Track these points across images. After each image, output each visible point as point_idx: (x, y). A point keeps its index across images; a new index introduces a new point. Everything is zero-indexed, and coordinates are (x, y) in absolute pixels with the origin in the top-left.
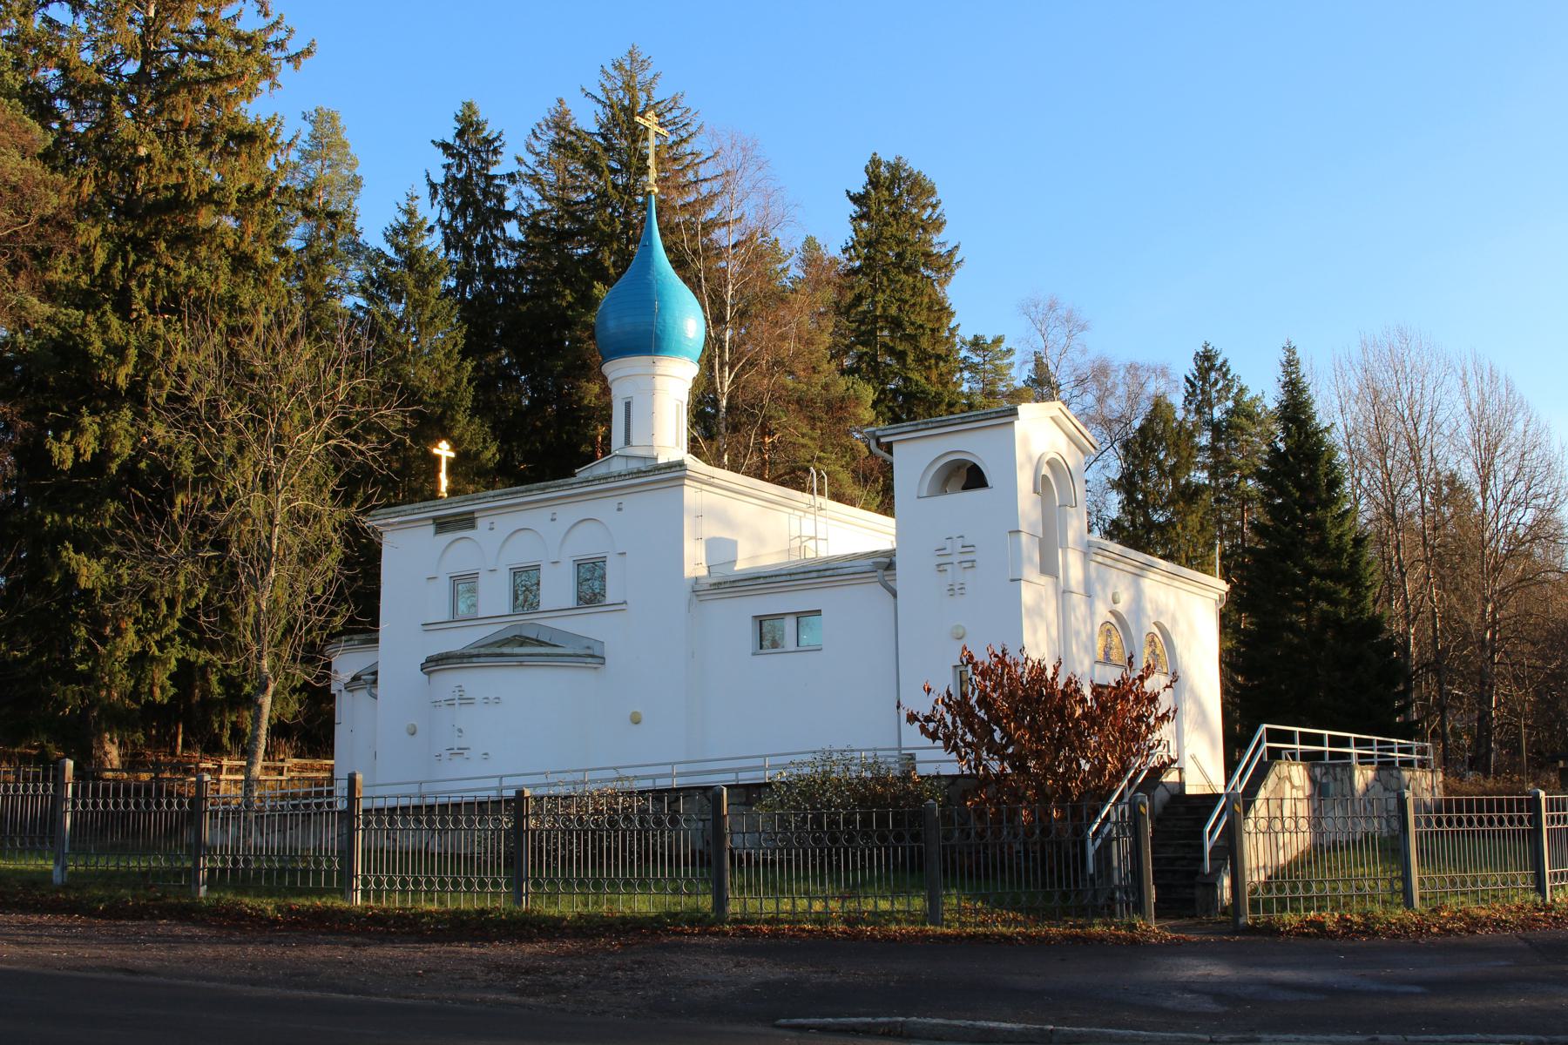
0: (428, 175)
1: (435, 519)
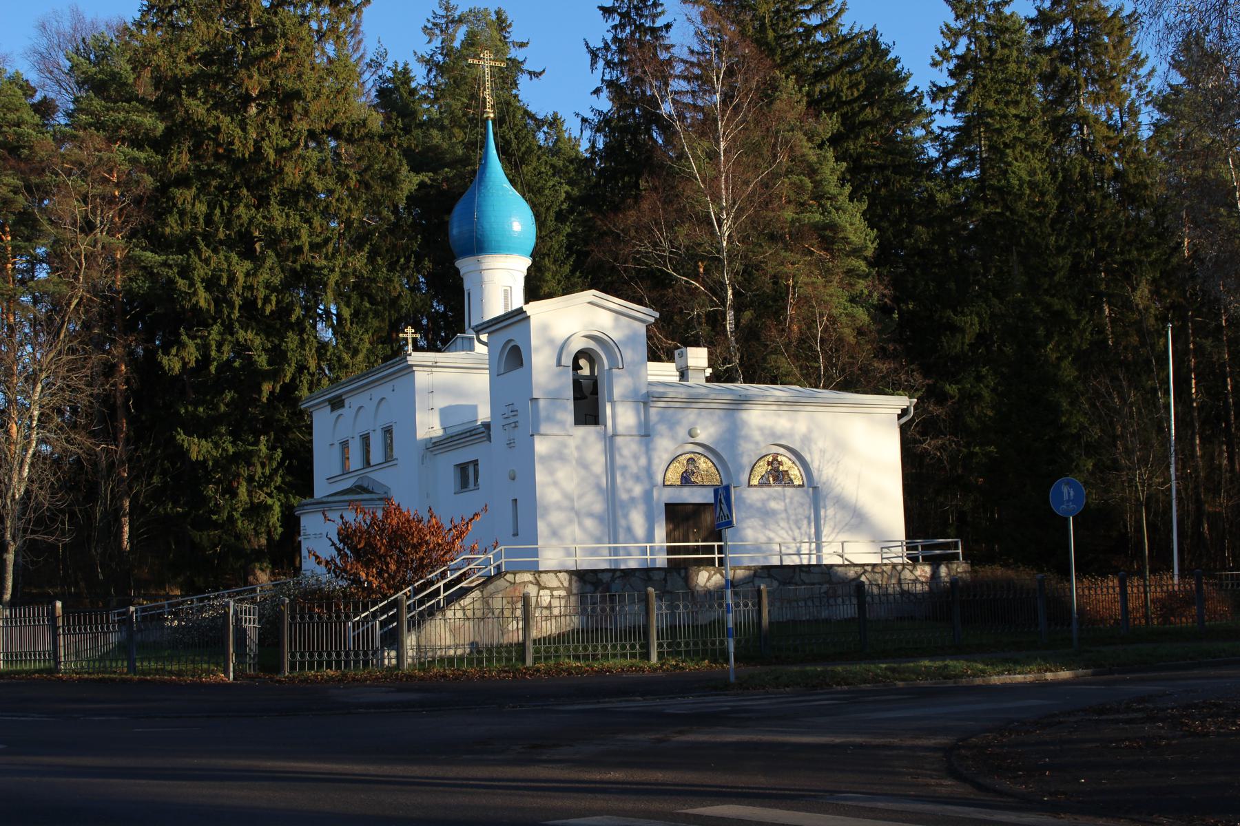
0: (587, 44)
1: (330, 401)
